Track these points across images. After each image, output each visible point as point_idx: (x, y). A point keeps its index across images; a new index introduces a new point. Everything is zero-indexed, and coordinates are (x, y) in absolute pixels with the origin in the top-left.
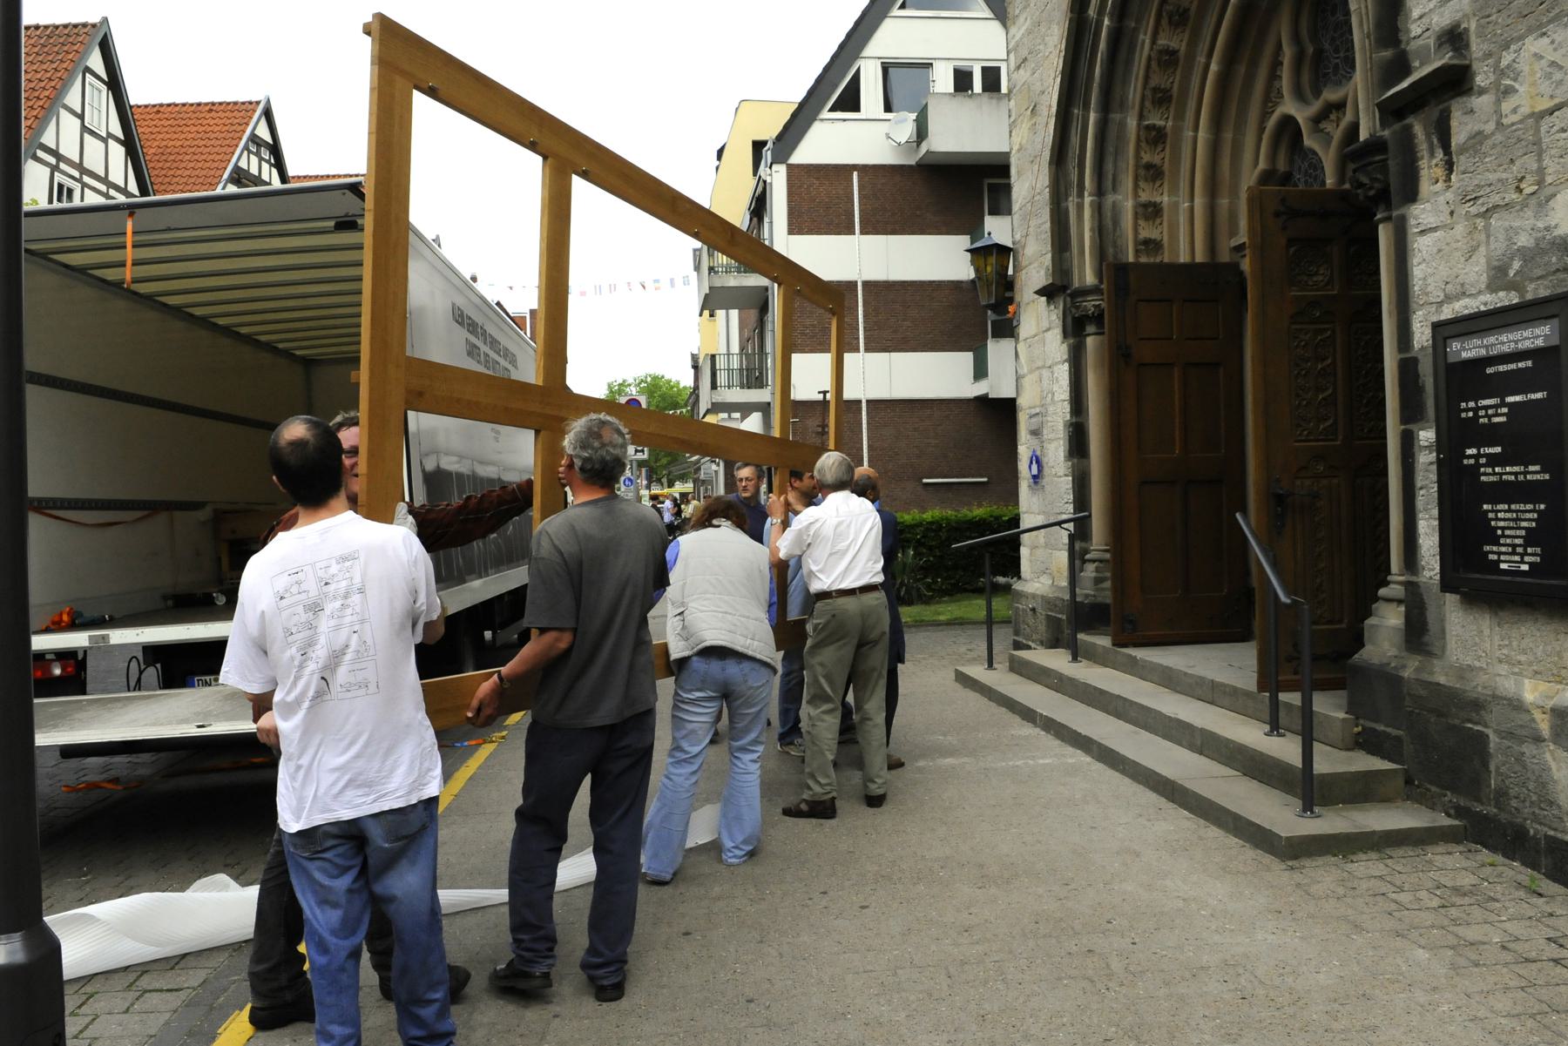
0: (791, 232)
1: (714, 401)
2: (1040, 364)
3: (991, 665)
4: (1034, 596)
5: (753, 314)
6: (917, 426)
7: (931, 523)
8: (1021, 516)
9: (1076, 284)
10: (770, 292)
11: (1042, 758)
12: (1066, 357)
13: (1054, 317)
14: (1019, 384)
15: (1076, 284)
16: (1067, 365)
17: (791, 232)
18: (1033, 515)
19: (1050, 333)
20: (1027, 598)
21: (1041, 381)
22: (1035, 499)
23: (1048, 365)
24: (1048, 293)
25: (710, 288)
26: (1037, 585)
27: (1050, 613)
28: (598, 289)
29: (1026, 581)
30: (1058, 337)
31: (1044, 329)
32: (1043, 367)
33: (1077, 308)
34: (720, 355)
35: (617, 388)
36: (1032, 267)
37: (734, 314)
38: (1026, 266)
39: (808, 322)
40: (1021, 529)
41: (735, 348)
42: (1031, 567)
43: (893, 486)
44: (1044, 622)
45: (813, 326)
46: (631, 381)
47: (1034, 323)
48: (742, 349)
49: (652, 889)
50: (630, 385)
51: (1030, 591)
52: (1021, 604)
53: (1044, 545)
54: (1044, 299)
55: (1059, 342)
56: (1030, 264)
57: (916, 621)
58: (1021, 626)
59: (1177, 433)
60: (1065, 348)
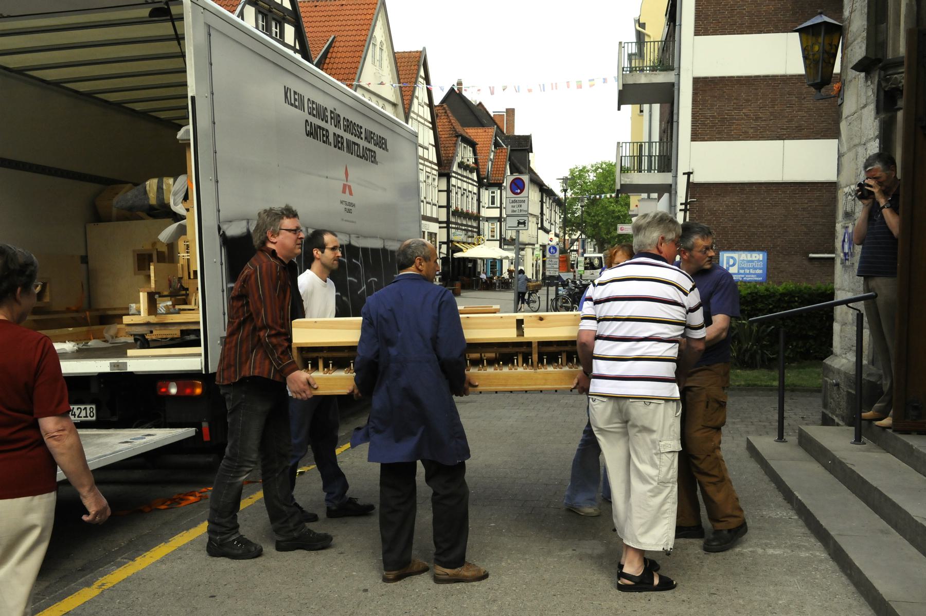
0: (697, 33)
1: (623, 183)
2: (856, 141)
3: (781, 438)
4: (839, 371)
5: (668, 106)
6: (806, 206)
7: (783, 295)
8: (836, 292)
9: (890, 56)
10: (676, 87)
11: (774, 548)
12: (877, 133)
13: (870, 93)
14: (840, 163)
15: (890, 56)
16: (878, 141)
17: (697, 33)
18: (844, 292)
19: (866, 109)
20: (834, 373)
21: (857, 160)
22: (846, 276)
23: (863, 143)
24: (864, 66)
25: (623, 85)
26: (844, 361)
27: (850, 390)
28: (555, 86)
29: (836, 356)
30: (873, 112)
31: (862, 106)
32: (860, 144)
33: (887, 81)
34: (645, 143)
35: (577, 173)
36: (856, 42)
37: (656, 107)
38: (852, 43)
39: (709, 113)
40: (835, 300)
41: (656, 137)
42: (841, 342)
43: (780, 259)
44: (845, 398)
45: (713, 117)
46: (589, 167)
47: (854, 99)
48: (661, 139)
49: (720, 557)
50: (588, 171)
51: (836, 366)
52: (829, 378)
53: (851, 322)
54: (863, 74)
55: (873, 118)
56: (855, 40)
57: (749, 385)
58: (829, 399)
59: (501, 142)
60: (877, 123)
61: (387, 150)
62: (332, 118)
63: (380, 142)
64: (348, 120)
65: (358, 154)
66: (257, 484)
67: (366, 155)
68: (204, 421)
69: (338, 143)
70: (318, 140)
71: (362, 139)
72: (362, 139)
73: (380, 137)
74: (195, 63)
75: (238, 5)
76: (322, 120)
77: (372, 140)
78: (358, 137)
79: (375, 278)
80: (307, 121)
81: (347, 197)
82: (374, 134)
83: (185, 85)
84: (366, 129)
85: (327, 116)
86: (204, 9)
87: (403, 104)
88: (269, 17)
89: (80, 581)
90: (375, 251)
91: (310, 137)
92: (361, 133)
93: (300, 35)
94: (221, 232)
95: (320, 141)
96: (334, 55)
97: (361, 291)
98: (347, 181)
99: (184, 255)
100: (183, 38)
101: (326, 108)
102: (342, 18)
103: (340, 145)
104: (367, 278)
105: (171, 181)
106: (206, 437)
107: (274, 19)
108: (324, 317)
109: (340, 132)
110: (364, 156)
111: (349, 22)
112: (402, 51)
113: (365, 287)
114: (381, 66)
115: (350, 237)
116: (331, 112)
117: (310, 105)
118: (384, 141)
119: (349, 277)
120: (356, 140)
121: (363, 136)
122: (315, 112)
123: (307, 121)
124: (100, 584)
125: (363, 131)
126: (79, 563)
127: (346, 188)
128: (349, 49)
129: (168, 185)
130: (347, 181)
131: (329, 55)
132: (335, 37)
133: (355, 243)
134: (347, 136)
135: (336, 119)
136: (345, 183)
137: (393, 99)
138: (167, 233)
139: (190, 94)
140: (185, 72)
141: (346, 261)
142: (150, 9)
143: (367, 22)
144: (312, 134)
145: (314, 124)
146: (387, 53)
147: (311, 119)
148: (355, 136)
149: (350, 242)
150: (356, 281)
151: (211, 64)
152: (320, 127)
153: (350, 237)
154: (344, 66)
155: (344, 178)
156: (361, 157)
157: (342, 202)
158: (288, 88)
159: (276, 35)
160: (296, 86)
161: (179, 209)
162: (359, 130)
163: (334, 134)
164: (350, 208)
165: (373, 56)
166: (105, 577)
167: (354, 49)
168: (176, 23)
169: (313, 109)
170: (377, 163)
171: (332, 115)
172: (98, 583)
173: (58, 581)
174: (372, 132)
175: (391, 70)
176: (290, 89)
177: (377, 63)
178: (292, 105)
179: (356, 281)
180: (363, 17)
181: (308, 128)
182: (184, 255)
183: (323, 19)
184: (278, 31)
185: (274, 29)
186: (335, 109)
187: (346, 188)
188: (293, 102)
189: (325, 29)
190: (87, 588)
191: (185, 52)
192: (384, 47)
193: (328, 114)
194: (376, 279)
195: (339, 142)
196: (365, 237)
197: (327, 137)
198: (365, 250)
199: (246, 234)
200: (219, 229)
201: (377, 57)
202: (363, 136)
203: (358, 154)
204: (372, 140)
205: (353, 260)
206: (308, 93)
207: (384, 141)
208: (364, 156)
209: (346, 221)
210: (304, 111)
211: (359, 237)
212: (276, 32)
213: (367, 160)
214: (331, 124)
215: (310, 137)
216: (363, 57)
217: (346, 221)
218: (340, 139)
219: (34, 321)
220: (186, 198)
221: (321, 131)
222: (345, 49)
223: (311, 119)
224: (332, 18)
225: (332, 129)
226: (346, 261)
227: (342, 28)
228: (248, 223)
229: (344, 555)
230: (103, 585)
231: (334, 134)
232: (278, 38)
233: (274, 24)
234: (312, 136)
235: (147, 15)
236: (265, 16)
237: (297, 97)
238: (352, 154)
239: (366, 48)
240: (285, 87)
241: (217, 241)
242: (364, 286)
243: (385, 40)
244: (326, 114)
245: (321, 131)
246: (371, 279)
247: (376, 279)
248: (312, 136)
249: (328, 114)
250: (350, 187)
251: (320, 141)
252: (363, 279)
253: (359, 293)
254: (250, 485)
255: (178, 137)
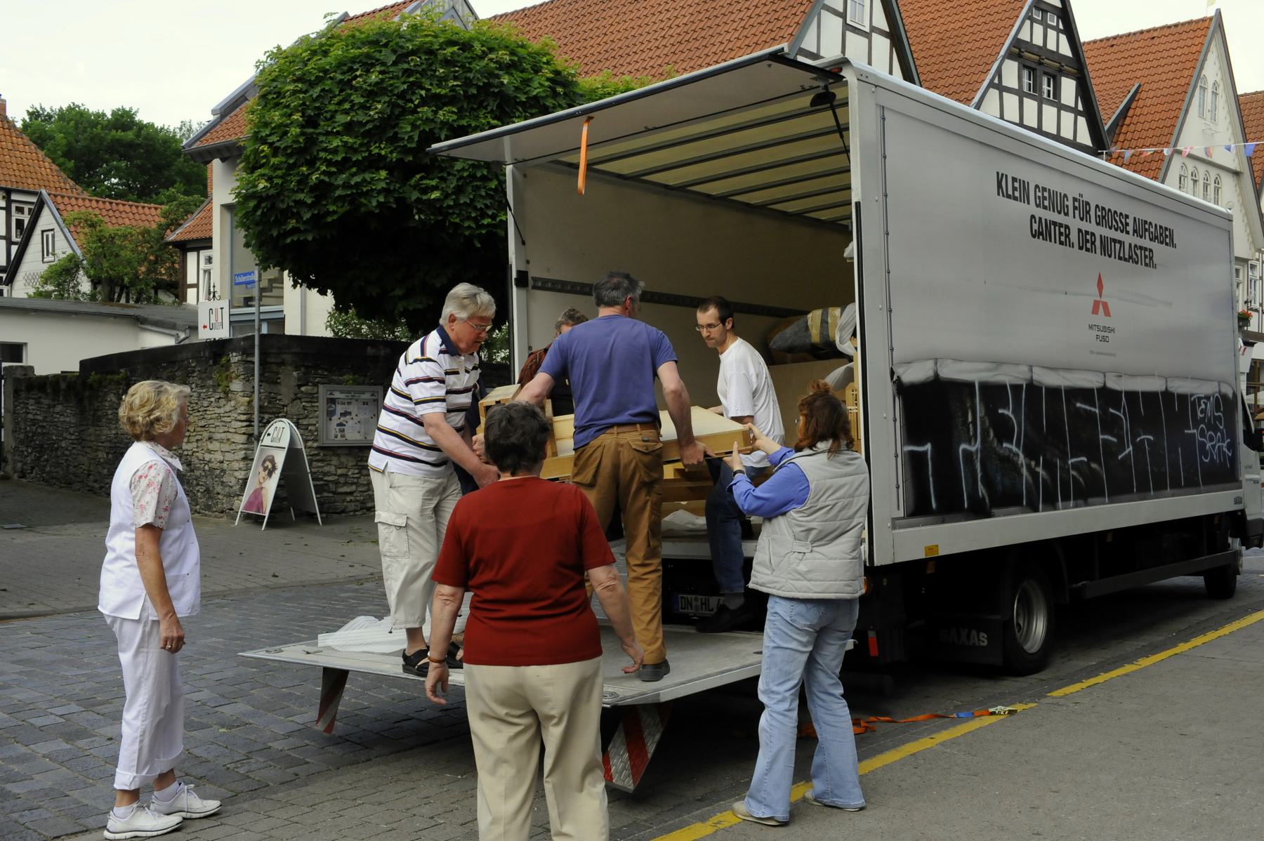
61: (1174, 246)
62: (1075, 208)
63: (1161, 234)
64: (1103, 209)
65: (1122, 255)
66: (947, 719)
67: (1134, 256)
68: (871, 630)
69: (1086, 242)
70: (1051, 241)
71: (1128, 233)
72: (1128, 233)
73: (1161, 227)
74: (861, 158)
75: (993, 62)
76: (1059, 212)
77: (1147, 233)
78: (1122, 232)
79: (1149, 435)
80: (1033, 217)
81: (1101, 319)
82: (1150, 223)
83: (848, 188)
84: (1135, 218)
85: (1067, 206)
86: (876, 86)
87: (1252, 172)
88: (1038, 71)
89: (696, 813)
90: (1150, 397)
91: (1039, 238)
92: (1127, 224)
93: (1084, 90)
94: (895, 378)
95: (1055, 242)
96: (1138, 111)
97: (1124, 454)
98: (1101, 296)
99: (852, 408)
100: (847, 129)
101: (1065, 196)
102: (1151, 57)
103: (1089, 245)
104: (1135, 436)
105: (837, 311)
106: (874, 651)
107: (1045, 73)
108: (313, 480)
109: (1091, 227)
110: (1131, 257)
111: (1163, 62)
112: (1254, 91)
113: (1131, 448)
114: (1214, 119)
115: (1105, 376)
116: (1075, 200)
117: (1039, 194)
118: (1167, 233)
119: (1102, 434)
120: (1118, 235)
121: (1130, 228)
122: (1046, 203)
123: (1033, 217)
124: (715, 821)
125: (1130, 221)
126: (700, 792)
127: (1099, 307)
128: (1164, 100)
129: (835, 317)
130: (1101, 296)
131: (1130, 113)
132: (1140, 86)
133: (1113, 384)
134: (1101, 231)
135: (1083, 209)
136: (1098, 299)
137: (1233, 165)
138: (833, 376)
139: (854, 201)
140: (849, 171)
141: (1097, 411)
142: (812, 96)
143: (1191, 57)
144: (1041, 234)
145: (1046, 220)
146: (1224, 98)
147: (1040, 213)
148: (1116, 230)
149: (1105, 383)
150: (1115, 440)
151: (885, 157)
152: (1055, 224)
153: (1105, 376)
154: (1154, 125)
155: (1096, 290)
156: (1126, 260)
157: (1091, 327)
158: (1002, 175)
159: (1049, 96)
160: (1014, 169)
161: (846, 347)
162: (1123, 220)
163: (1080, 231)
164: (1106, 334)
165: (1202, 106)
166: (724, 813)
167: (1169, 99)
168: (837, 111)
169: (1044, 198)
170: (1155, 267)
171: (1077, 204)
172: (714, 819)
173: (671, 809)
174: (1146, 222)
175: (1231, 123)
176: (1006, 176)
177: (1207, 115)
178: (1008, 196)
179: (1115, 440)
180: (1186, 50)
181: (1035, 226)
182: (852, 408)
183: (1123, 62)
184: (1051, 89)
185: (1045, 87)
186: (1081, 195)
187: (1099, 307)
188: (1010, 192)
189: (1125, 76)
190: (700, 824)
191: (849, 146)
192: (1220, 91)
193: (1070, 203)
194: (1151, 438)
195: (1087, 241)
196: (1132, 376)
197: (1067, 236)
198: (1132, 395)
199: (932, 379)
200: (892, 373)
201: (1208, 105)
202: (1130, 228)
203: (1122, 255)
204: (1147, 233)
205: (1111, 410)
206: (1034, 177)
207: (1167, 233)
208: (1131, 257)
209: (1098, 353)
210: (1029, 203)
211: (1121, 376)
212: (1049, 91)
213: (1137, 263)
214: (1074, 217)
215: (1039, 238)
216: (1184, 108)
217: (1098, 353)
218: (1088, 237)
219: (690, 488)
220: (854, 335)
221: (1057, 228)
222: (1155, 101)
223: (1040, 213)
224: (1137, 59)
225: (1075, 223)
226: (1097, 411)
227: (1153, 71)
228: (936, 364)
229: (1041, 837)
230: (719, 822)
231: (1080, 231)
232: (1051, 98)
233: (1045, 80)
234: (1041, 237)
235: (808, 104)
236: (1032, 70)
237: (1017, 185)
238: (1110, 256)
239: (1188, 96)
240: (998, 173)
241: (889, 388)
242: (1128, 447)
243: (1222, 79)
244: (1066, 203)
245: (1057, 228)
246: (1143, 437)
247: (1151, 438)
248: (1041, 237)
249: (1070, 203)
250: (1105, 305)
251: (1055, 242)
252: (1127, 437)
253: (1120, 457)
254: (937, 719)
255: (845, 255)
